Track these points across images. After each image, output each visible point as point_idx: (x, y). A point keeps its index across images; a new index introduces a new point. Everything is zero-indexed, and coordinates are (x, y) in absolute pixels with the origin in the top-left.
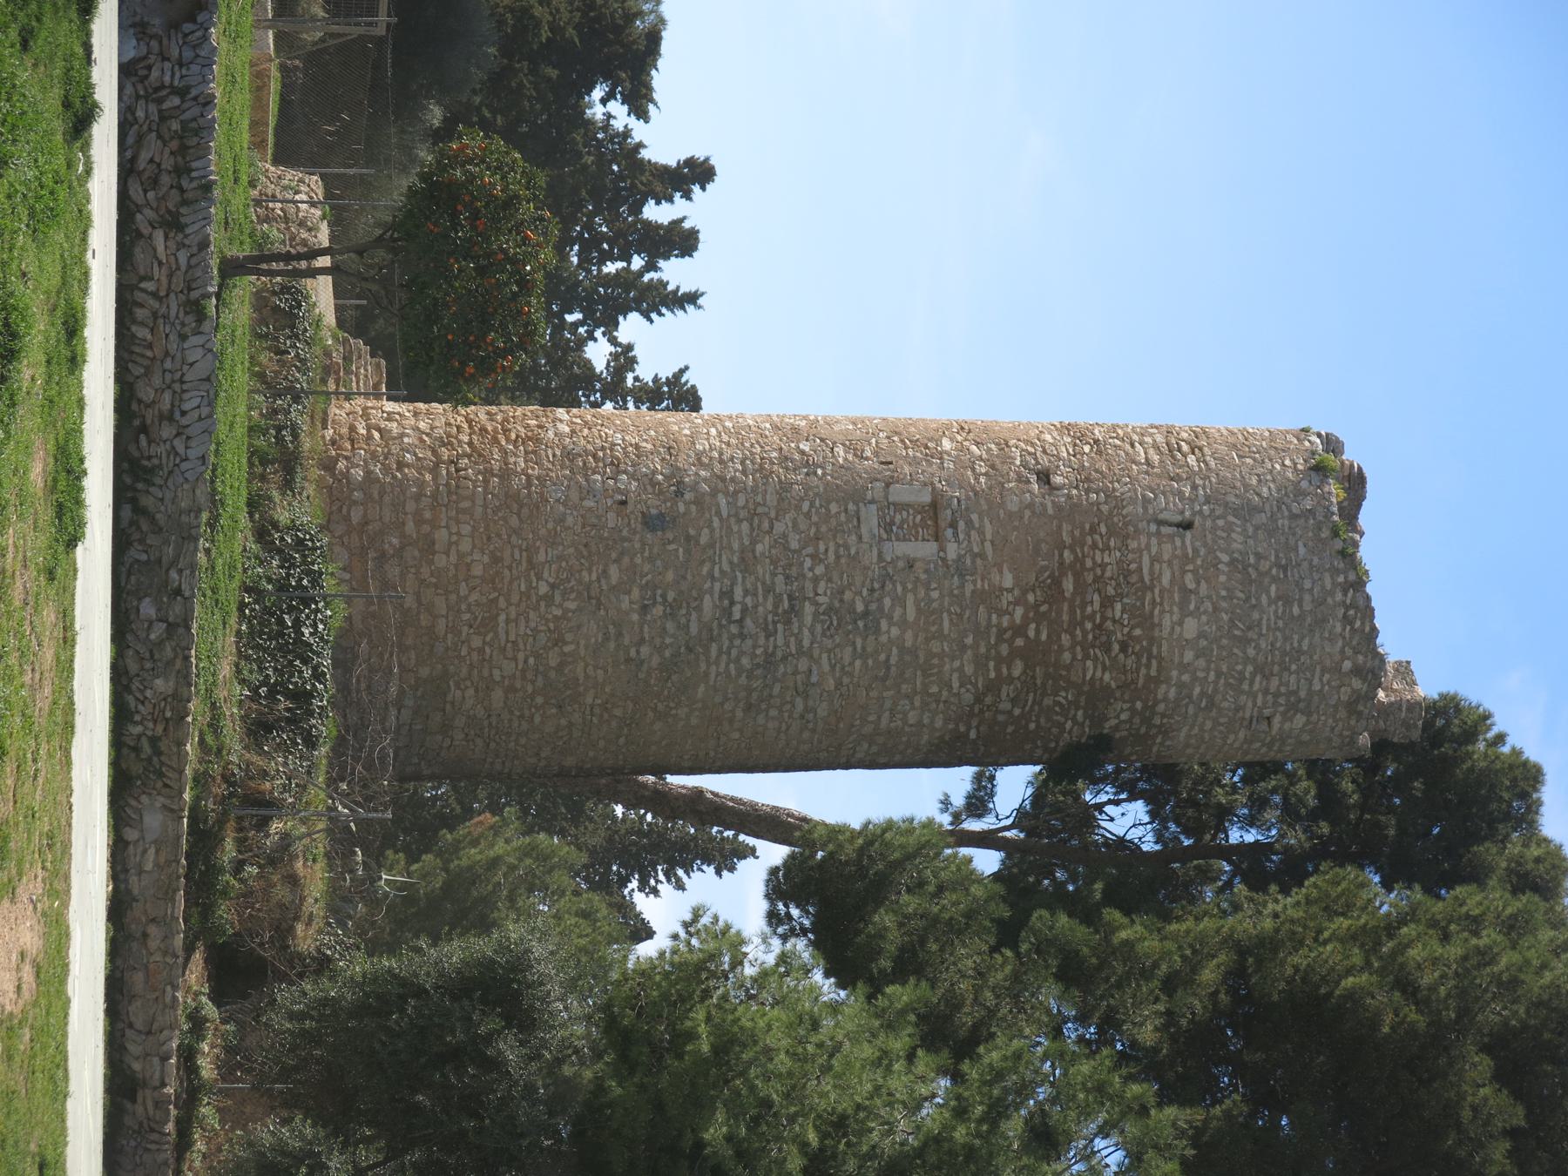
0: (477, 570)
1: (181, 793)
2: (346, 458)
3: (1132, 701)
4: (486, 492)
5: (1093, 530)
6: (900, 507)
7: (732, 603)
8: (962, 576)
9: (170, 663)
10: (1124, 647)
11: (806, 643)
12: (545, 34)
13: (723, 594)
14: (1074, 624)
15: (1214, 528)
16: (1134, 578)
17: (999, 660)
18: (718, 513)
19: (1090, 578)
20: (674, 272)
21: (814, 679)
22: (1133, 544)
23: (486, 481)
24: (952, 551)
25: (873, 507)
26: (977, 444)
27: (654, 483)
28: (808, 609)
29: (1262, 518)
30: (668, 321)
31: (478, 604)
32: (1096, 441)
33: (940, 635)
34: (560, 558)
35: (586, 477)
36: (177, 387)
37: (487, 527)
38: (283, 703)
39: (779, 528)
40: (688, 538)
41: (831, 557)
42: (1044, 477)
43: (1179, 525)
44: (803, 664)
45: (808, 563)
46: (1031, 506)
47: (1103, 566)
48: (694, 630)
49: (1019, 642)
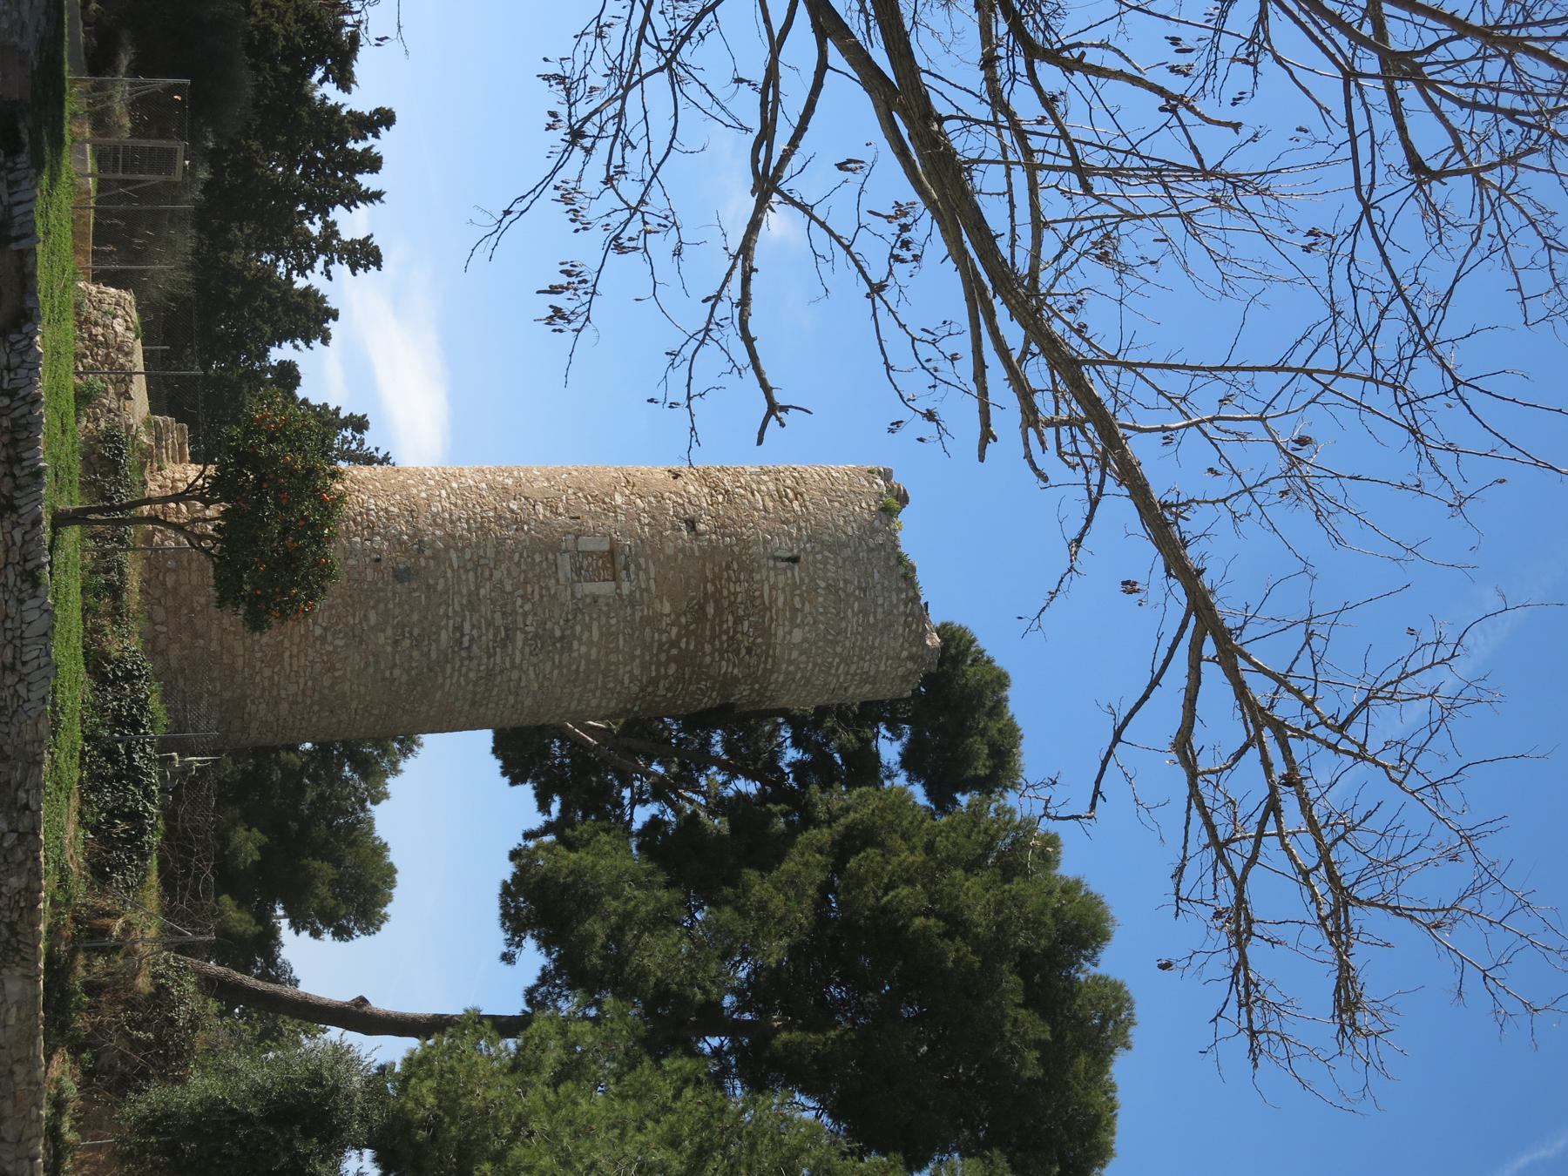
1: (36, 963)
3: (752, 684)
5: (728, 567)
6: (589, 554)
7: (462, 635)
8: (633, 607)
9: (21, 864)
10: (749, 651)
11: (518, 661)
12: (281, 43)
13: (455, 629)
14: (714, 637)
15: (814, 562)
16: (757, 603)
17: (659, 665)
18: (451, 566)
19: (726, 604)
20: (366, 180)
21: (523, 684)
22: (757, 577)
24: (626, 588)
25: (567, 556)
26: (641, 497)
27: (401, 543)
28: (520, 636)
29: (848, 552)
30: (363, 210)
31: (268, 645)
32: (727, 491)
33: (617, 650)
34: (331, 607)
35: (349, 539)
36: (17, 642)
39: (497, 575)
40: (428, 587)
41: (537, 597)
42: (691, 524)
43: (788, 560)
44: (515, 675)
45: (519, 602)
46: (683, 550)
47: (736, 594)
48: (434, 655)
49: (674, 651)
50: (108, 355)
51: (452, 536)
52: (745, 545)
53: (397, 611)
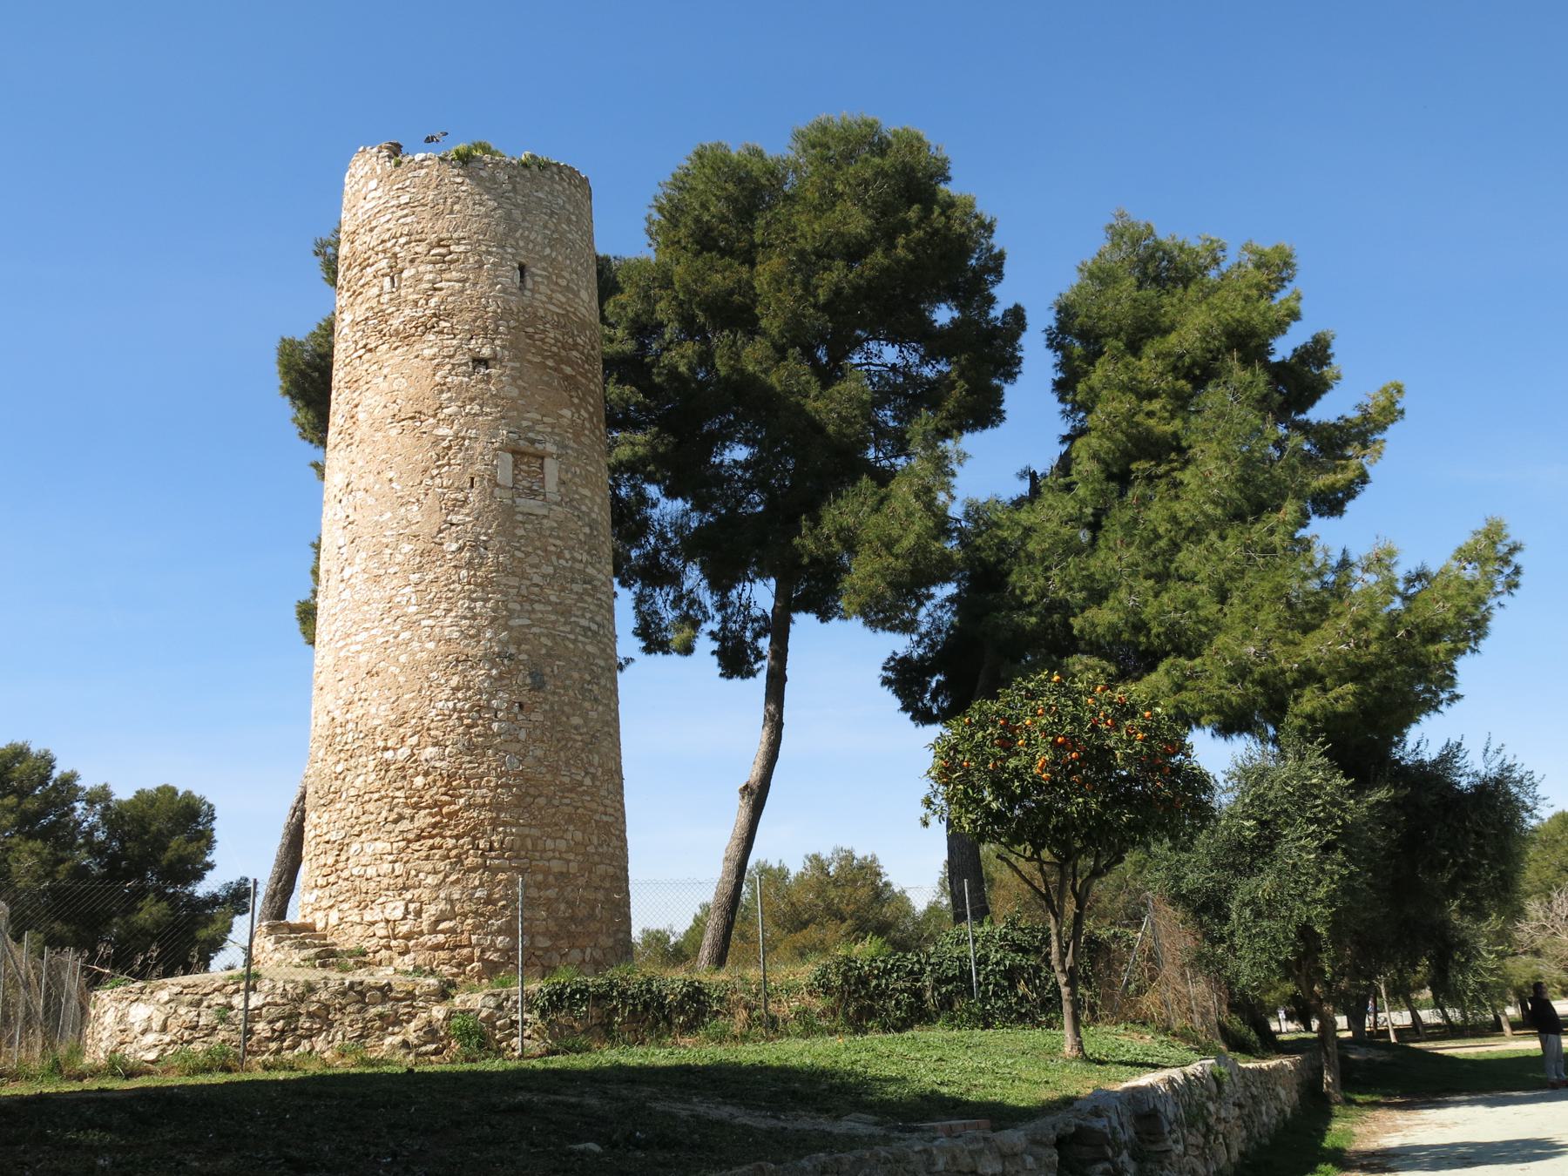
0: (579, 836)
2: (483, 952)
4: (517, 825)
5: (530, 337)
6: (515, 481)
18: (528, 626)
23: (505, 824)
24: (550, 448)
25: (518, 500)
27: (500, 677)
29: (517, 213)
34: (567, 763)
37: (548, 825)
38: (1022, 988)
39: (537, 579)
40: (549, 655)
41: (558, 542)
42: (479, 362)
43: (522, 276)
46: (514, 379)
47: (555, 339)
50: (310, 1015)
51: (493, 620)
52: (507, 313)
53: (571, 693)
